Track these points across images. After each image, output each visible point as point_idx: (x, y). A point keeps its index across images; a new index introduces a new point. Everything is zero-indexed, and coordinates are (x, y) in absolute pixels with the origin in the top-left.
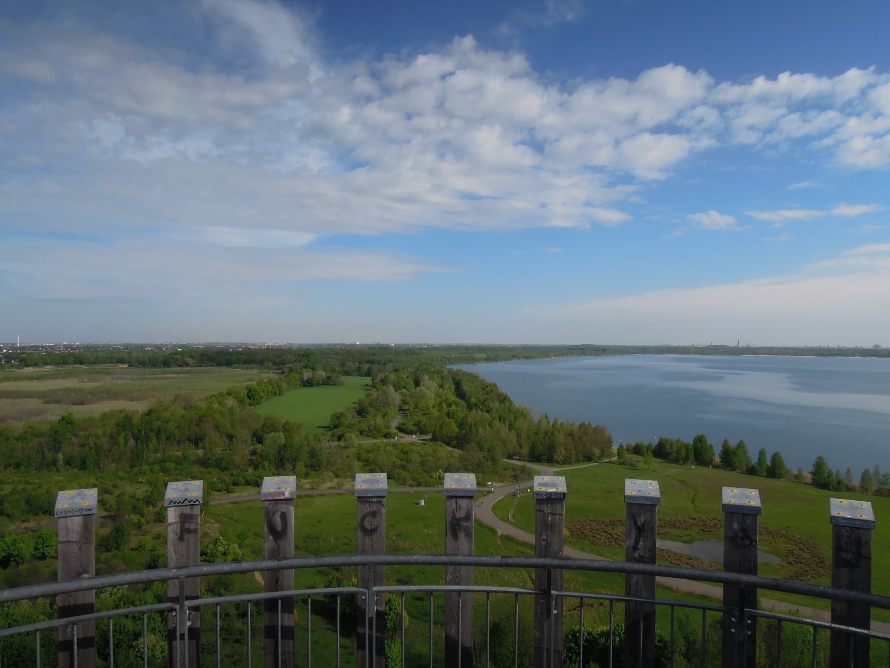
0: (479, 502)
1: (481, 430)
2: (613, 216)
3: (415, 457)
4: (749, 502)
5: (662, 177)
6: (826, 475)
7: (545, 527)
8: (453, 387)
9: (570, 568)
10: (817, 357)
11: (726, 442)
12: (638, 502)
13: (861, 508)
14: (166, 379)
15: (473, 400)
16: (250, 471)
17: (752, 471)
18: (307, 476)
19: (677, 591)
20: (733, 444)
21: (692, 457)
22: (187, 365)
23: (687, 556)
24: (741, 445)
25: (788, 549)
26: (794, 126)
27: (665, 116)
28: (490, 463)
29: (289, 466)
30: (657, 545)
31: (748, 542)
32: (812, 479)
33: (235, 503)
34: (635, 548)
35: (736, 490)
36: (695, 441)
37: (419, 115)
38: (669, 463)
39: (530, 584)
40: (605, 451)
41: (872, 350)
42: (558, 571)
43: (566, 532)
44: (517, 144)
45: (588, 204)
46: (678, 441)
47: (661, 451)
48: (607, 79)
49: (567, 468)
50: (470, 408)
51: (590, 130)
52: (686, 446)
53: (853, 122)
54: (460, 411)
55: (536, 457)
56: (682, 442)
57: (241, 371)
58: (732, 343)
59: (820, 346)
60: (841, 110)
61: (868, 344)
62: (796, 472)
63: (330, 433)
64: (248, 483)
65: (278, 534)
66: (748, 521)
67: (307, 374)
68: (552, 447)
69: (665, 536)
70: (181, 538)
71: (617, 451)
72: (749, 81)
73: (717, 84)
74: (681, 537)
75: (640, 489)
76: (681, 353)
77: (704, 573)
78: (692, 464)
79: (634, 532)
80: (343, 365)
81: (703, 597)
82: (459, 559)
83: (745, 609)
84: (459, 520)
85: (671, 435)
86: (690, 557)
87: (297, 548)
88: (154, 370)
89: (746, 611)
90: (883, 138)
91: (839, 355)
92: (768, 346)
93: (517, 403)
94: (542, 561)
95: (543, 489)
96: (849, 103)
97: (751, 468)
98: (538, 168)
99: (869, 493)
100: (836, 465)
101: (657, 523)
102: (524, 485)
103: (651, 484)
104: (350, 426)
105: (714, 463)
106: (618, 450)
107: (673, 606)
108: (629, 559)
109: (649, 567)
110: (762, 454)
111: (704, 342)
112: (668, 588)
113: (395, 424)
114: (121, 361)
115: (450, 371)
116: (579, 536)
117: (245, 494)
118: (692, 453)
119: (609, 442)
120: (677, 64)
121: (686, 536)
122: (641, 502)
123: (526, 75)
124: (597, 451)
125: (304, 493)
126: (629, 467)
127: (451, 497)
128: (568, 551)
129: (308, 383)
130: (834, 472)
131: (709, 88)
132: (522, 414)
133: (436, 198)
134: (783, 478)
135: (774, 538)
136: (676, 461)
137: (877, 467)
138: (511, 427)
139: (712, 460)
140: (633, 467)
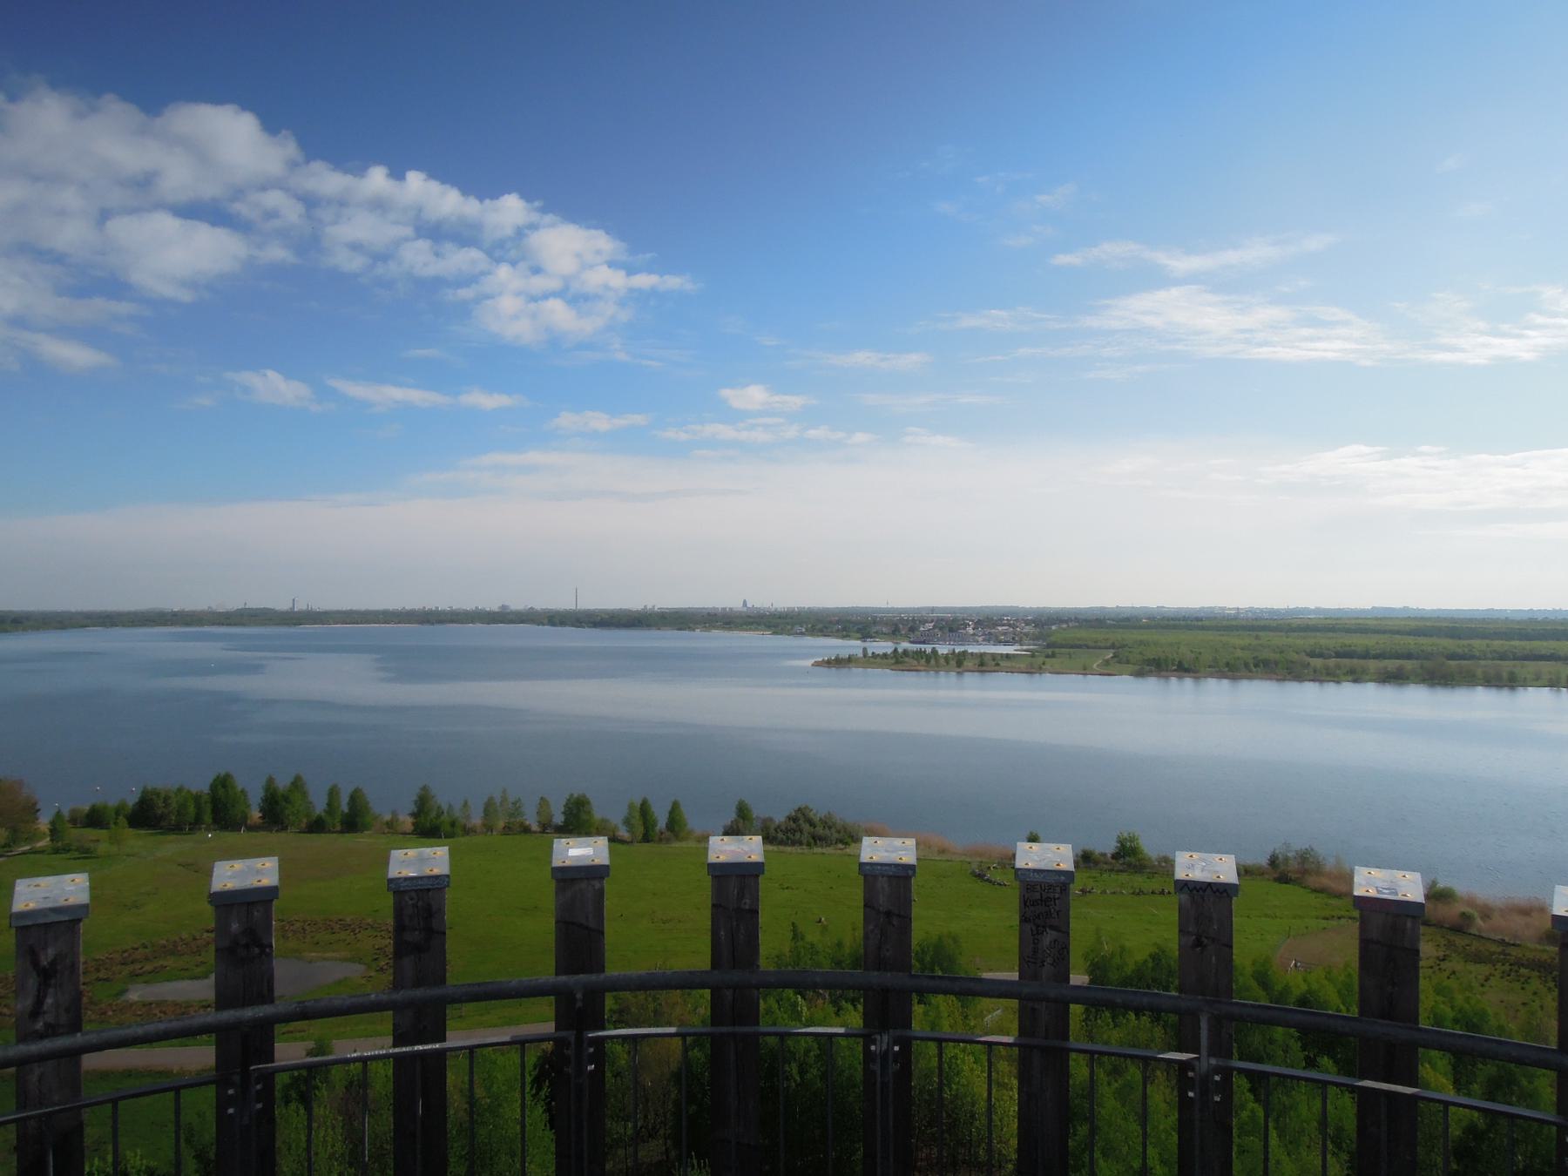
4: (259, 881)
5: (186, 296)
6: (433, 814)
10: (420, 626)
11: (270, 781)
12: (41, 921)
13: (434, 858)
20: (283, 783)
21: (208, 818)
23: (201, 1001)
24: (297, 784)
25: (377, 947)
26: (418, 257)
27: (210, 190)
31: (257, 950)
32: (413, 824)
34: (36, 1013)
35: (239, 865)
36: (213, 787)
38: (161, 834)
41: (498, 613)
46: (180, 790)
52: (197, 798)
53: (504, 271)
56: (189, 791)
58: (282, 605)
59: (424, 608)
60: (489, 253)
61: (493, 605)
62: (388, 817)
66: (256, 913)
71: (49, 826)
72: (360, 172)
73: (308, 162)
74: (187, 969)
75: (47, 895)
76: (187, 624)
78: (208, 830)
79: (32, 982)
83: (252, 1068)
86: (204, 1003)
89: (254, 1070)
90: (540, 302)
91: (452, 621)
92: (344, 609)
96: (501, 244)
97: (315, 822)
99: (494, 833)
100: (446, 798)
103: (73, 881)
105: (249, 822)
106: (53, 823)
111: (232, 603)
112: (104, 1075)
118: (208, 809)
119: (32, 810)
121: (197, 966)
122: (49, 920)
126: (76, 854)
130: (445, 807)
131: (293, 165)
134: (367, 830)
135: (355, 934)
136: (177, 829)
137: (504, 791)
139: (245, 817)
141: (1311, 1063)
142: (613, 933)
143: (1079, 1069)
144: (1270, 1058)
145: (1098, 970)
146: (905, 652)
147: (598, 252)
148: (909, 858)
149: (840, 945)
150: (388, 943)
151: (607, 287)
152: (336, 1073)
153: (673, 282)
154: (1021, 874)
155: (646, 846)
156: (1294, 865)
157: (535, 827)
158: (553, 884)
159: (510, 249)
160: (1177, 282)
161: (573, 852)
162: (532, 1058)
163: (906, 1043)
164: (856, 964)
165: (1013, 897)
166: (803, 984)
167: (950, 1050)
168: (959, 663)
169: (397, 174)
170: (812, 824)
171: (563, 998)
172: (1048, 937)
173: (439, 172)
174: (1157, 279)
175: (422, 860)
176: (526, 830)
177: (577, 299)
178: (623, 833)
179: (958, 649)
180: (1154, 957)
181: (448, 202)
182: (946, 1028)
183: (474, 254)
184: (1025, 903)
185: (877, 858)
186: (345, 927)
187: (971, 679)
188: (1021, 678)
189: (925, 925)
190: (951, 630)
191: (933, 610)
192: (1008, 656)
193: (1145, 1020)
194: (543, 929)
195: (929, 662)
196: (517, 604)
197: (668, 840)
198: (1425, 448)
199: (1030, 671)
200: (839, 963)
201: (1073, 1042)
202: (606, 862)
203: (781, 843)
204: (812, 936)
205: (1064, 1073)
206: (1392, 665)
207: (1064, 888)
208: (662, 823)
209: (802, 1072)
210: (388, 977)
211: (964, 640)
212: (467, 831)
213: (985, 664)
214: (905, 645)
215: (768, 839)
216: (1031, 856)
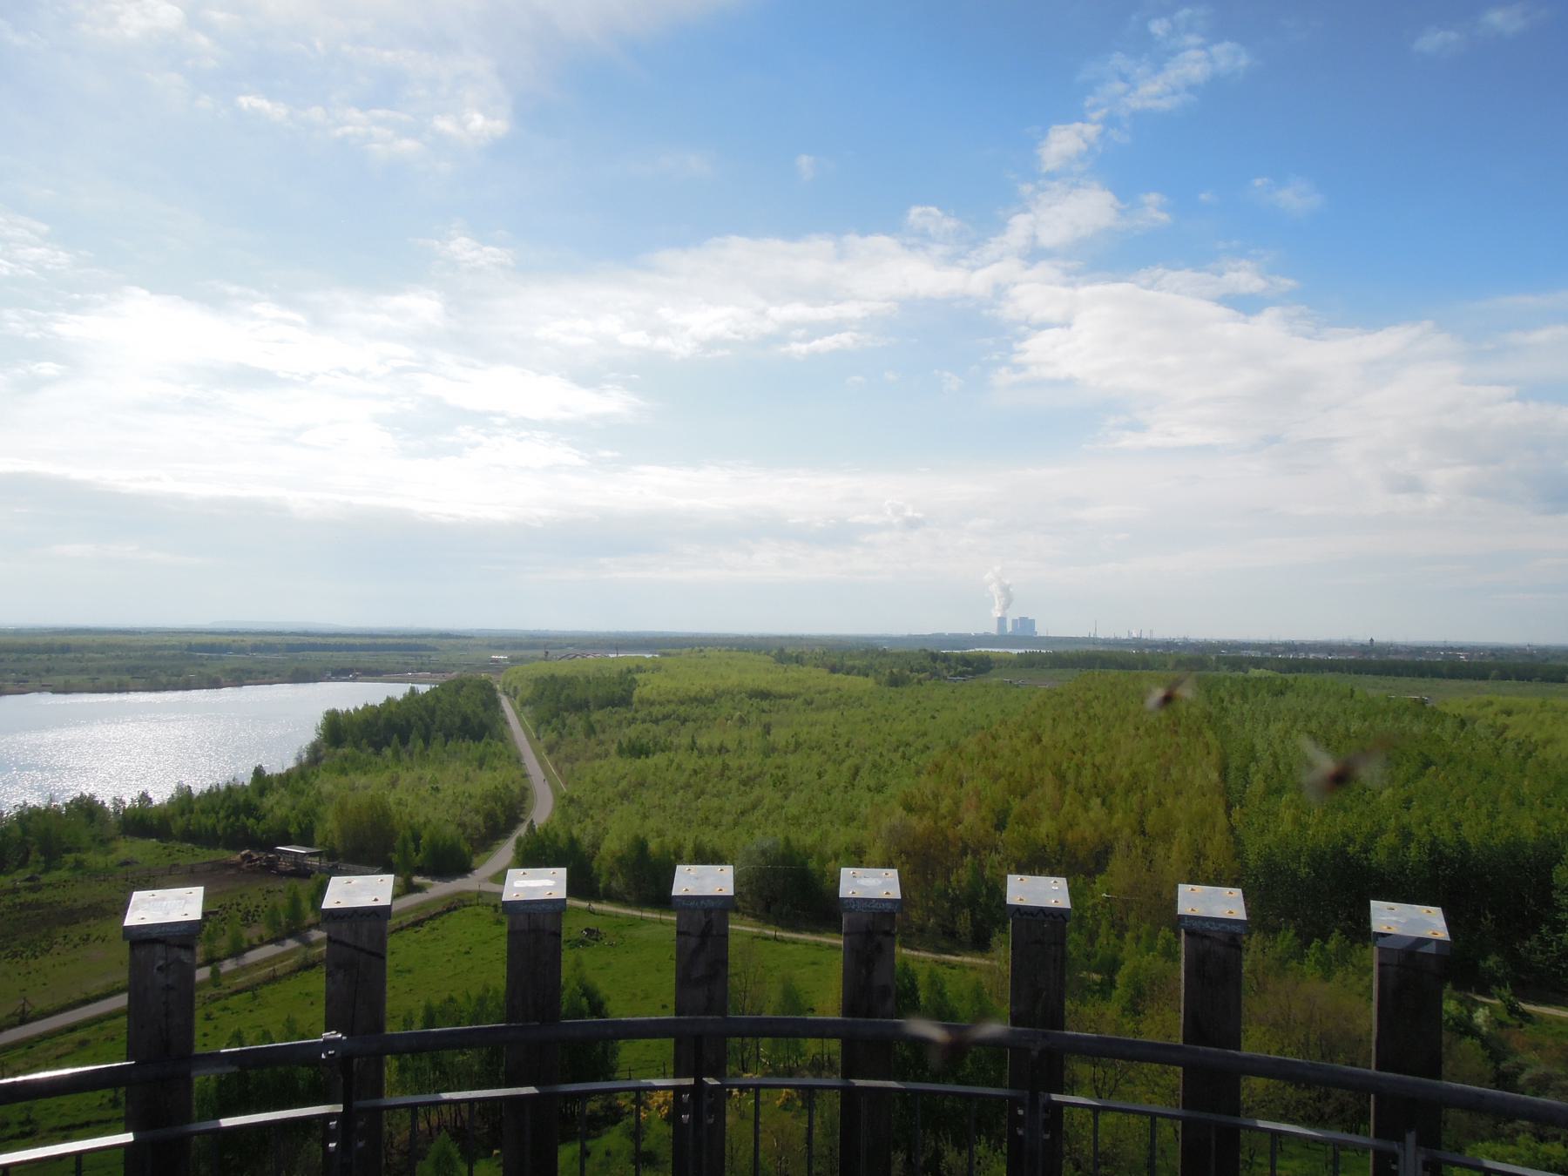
185: (694, 890)
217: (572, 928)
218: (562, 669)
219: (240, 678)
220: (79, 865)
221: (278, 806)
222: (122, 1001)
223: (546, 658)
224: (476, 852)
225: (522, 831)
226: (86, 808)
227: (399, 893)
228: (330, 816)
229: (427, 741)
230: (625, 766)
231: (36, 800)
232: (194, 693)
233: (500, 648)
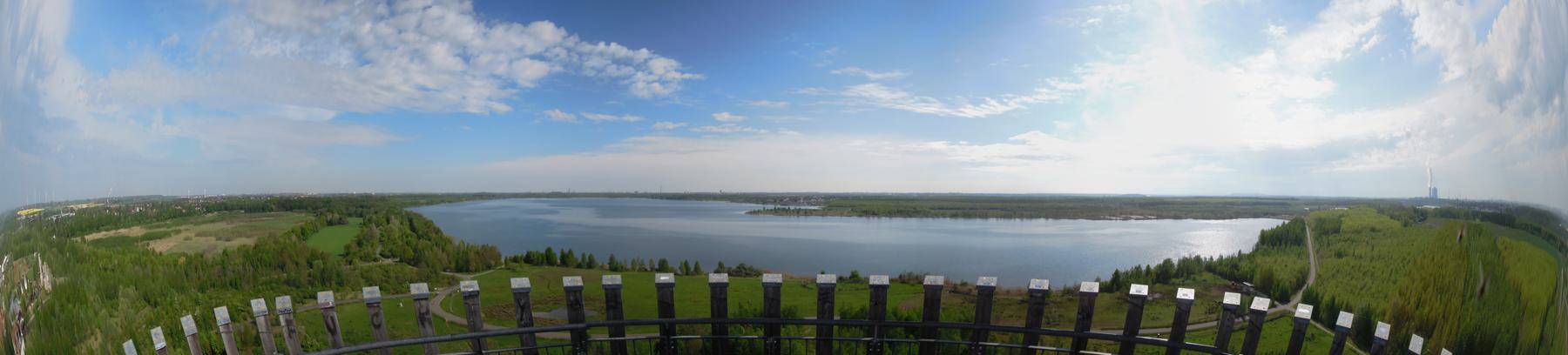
0: (432, 302)
1: (426, 253)
2: (502, 108)
3: (392, 274)
5: (532, 86)
7: (471, 314)
8: (408, 223)
9: (488, 336)
11: (562, 250)
14: (264, 221)
15: (420, 232)
16: (310, 288)
17: (579, 266)
18: (338, 290)
19: (548, 339)
20: (566, 251)
21: (545, 261)
22: (272, 210)
24: (570, 252)
26: (612, 70)
27: (538, 50)
28: (434, 275)
29: (328, 284)
30: (533, 315)
33: (307, 311)
34: (522, 319)
35: (570, 278)
37: (406, 31)
39: (470, 350)
40: (498, 263)
42: (483, 339)
43: (483, 315)
44: (455, 56)
45: (490, 99)
47: (528, 259)
48: (512, 22)
49: (477, 274)
50: (419, 238)
51: (497, 52)
52: (542, 255)
53: (640, 74)
54: (413, 240)
55: (459, 270)
57: (296, 215)
61: (632, 191)
62: (600, 264)
63: (344, 260)
64: (311, 297)
65: (333, 332)
67: (329, 217)
68: (467, 262)
69: (537, 310)
70: (290, 336)
72: (596, 44)
73: (569, 36)
77: (559, 327)
79: (519, 310)
80: (348, 209)
81: (561, 340)
82: (429, 339)
84: (423, 314)
85: (533, 249)
87: (344, 340)
88: (256, 214)
93: (446, 233)
94: (473, 334)
95: (466, 289)
96: (639, 65)
98: (464, 73)
100: (619, 259)
101: (531, 303)
102: (455, 288)
104: (355, 254)
107: (547, 347)
108: (520, 326)
109: (530, 329)
110: (583, 255)
111: (548, 190)
113: (378, 251)
114: (241, 209)
115: (406, 212)
116: (491, 316)
117: (311, 304)
119: (500, 256)
120: (551, 21)
123: (470, 13)
124: (493, 263)
125: (339, 303)
127: (416, 300)
128: (486, 326)
129: (330, 223)
131: (564, 38)
132: (448, 241)
133: (405, 88)
136: (537, 264)
138: (443, 250)
140: (514, 270)
141: (907, 337)
142: (677, 305)
143: (836, 345)
144: (895, 337)
145: (843, 315)
146: (779, 209)
147: (672, 66)
148: (780, 281)
149: (755, 310)
150: (605, 305)
151: (674, 78)
152: (593, 344)
153: (697, 76)
154: (818, 285)
155: (687, 277)
156: (907, 278)
157: (649, 269)
158: (656, 289)
159: (643, 66)
160: (872, 82)
161: (662, 278)
162: (653, 344)
163: (779, 340)
164: (761, 315)
165: (815, 294)
166: (744, 322)
167: (793, 342)
168: (798, 212)
169: (608, 44)
170: (745, 269)
171: (662, 325)
172: (827, 305)
173: (621, 43)
174: (866, 80)
175: (612, 279)
176: (646, 270)
177: (663, 82)
178: (679, 272)
179: (798, 207)
180: (861, 310)
181: (622, 51)
182: (792, 335)
183: (631, 69)
184: (820, 294)
185: (769, 281)
186: (591, 299)
187: (802, 218)
188: (820, 218)
189: (785, 302)
190: (796, 201)
191: (788, 193)
192: (815, 210)
193: (858, 329)
194: (653, 303)
195: (787, 212)
196: (641, 191)
197: (694, 275)
198: (961, 142)
199: (822, 215)
200: (755, 316)
201: (834, 338)
202: (673, 281)
203: (734, 276)
204: (746, 307)
205: (831, 347)
206: (954, 212)
207: (833, 289)
208: (692, 269)
209: (744, 349)
210: (605, 317)
211: (799, 204)
212: (627, 270)
213: (807, 213)
214: (779, 206)
215: (730, 275)
216: (823, 279)
217: (1309, 332)
218: (1323, 215)
219: (1238, 215)
220: (1194, 279)
221: (1245, 266)
222: (1189, 328)
223: (1319, 210)
224: (1292, 294)
225: (1305, 288)
226: (1198, 259)
227: (1272, 306)
228: (1258, 272)
229: (1286, 244)
230: (1335, 261)
231: (1187, 256)
232: (1226, 221)
233: (1307, 204)
